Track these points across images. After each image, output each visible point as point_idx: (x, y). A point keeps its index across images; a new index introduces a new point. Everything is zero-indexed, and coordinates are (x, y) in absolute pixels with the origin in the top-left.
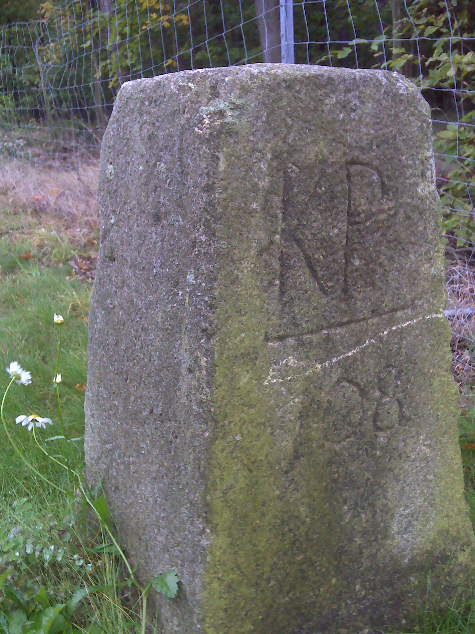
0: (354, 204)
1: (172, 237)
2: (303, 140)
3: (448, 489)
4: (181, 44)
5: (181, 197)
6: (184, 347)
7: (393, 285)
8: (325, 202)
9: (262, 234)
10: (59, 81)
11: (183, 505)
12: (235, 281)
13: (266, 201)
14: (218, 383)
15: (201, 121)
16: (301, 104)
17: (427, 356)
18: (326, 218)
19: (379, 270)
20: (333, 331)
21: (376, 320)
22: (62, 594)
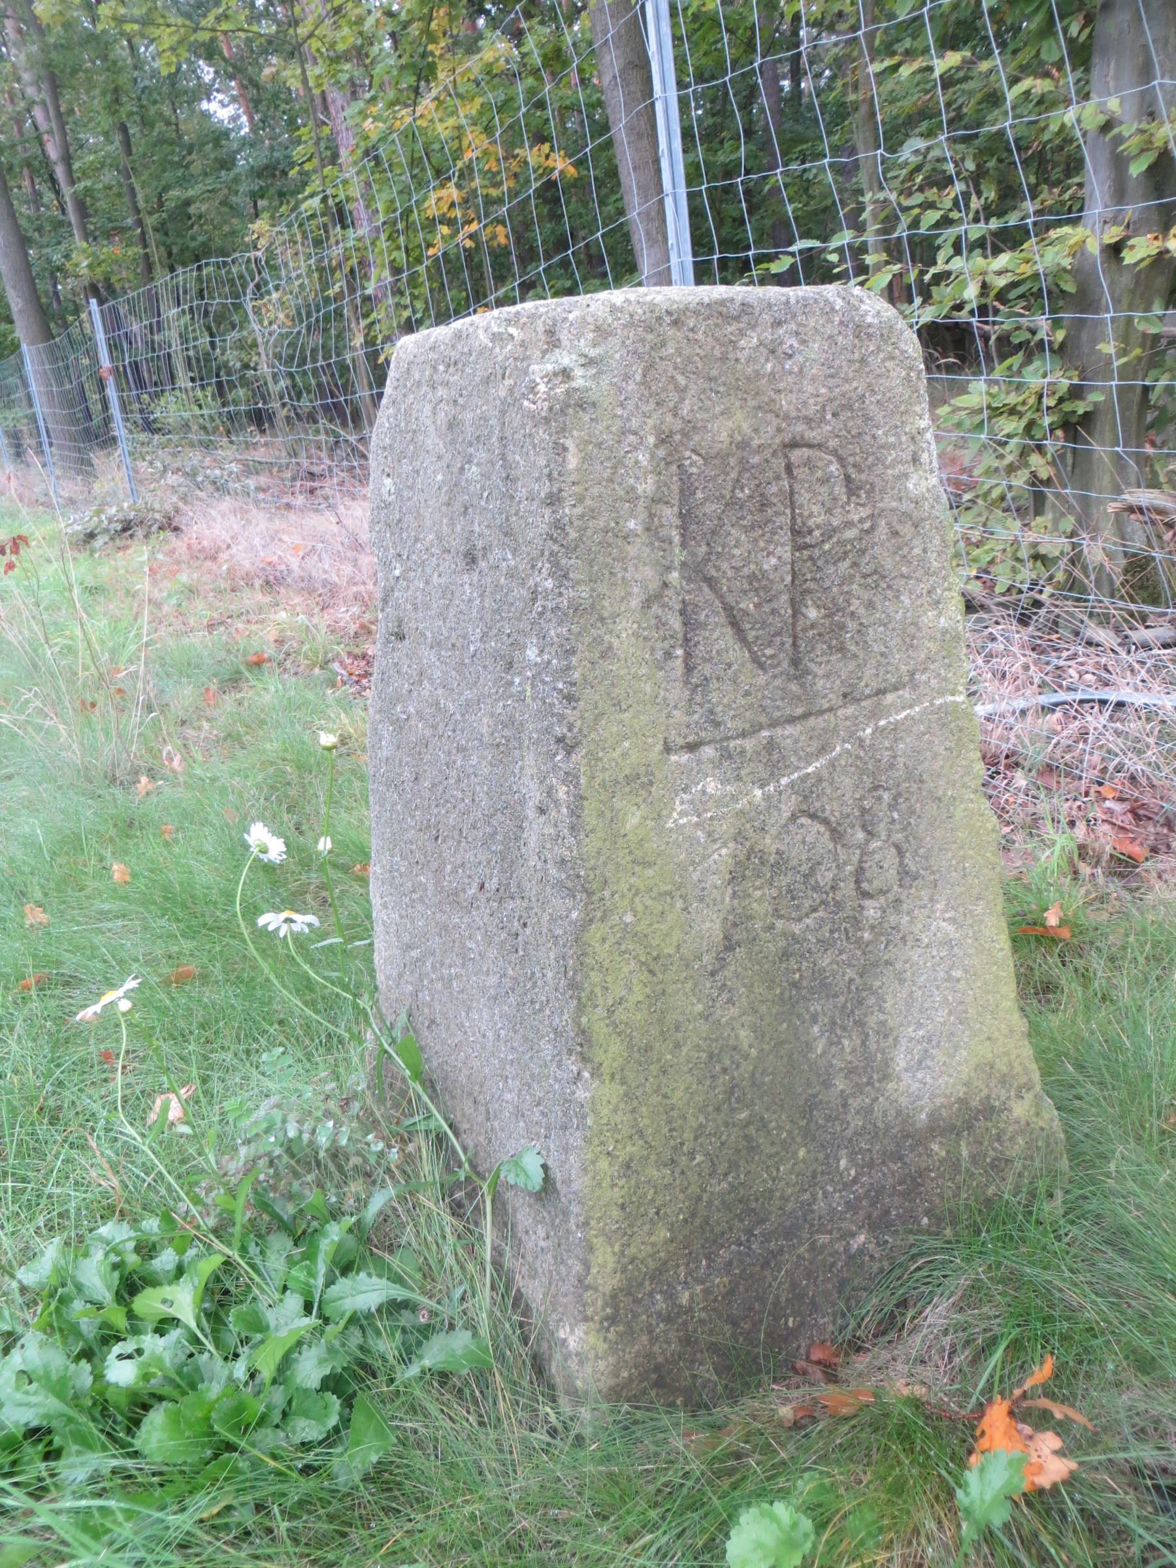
0: (801, 515)
1: (497, 587)
2: (707, 410)
3: (988, 992)
4: (500, 279)
5: (507, 520)
6: (529, 771)
7: (876, 648)
8: (752, 513)
9: (648, 572)
10: (292, 358)
11: (543, 1037)
12: (607, 653)
13: (651, 516)
14: (588, 828)
15: (533, 389)
16: (698, 351)
17: (942, 767)
18: (756, 540)
19: (851, 625)
20: (779, 731)
21: (850, 710)
22: (351, 1202)
